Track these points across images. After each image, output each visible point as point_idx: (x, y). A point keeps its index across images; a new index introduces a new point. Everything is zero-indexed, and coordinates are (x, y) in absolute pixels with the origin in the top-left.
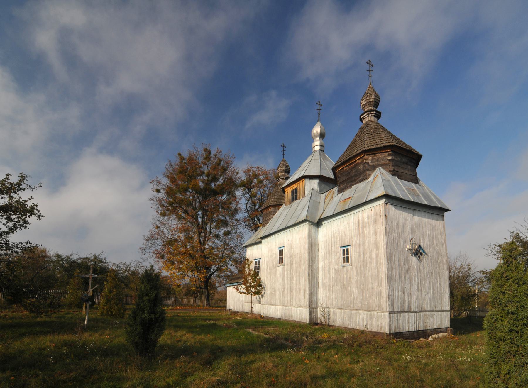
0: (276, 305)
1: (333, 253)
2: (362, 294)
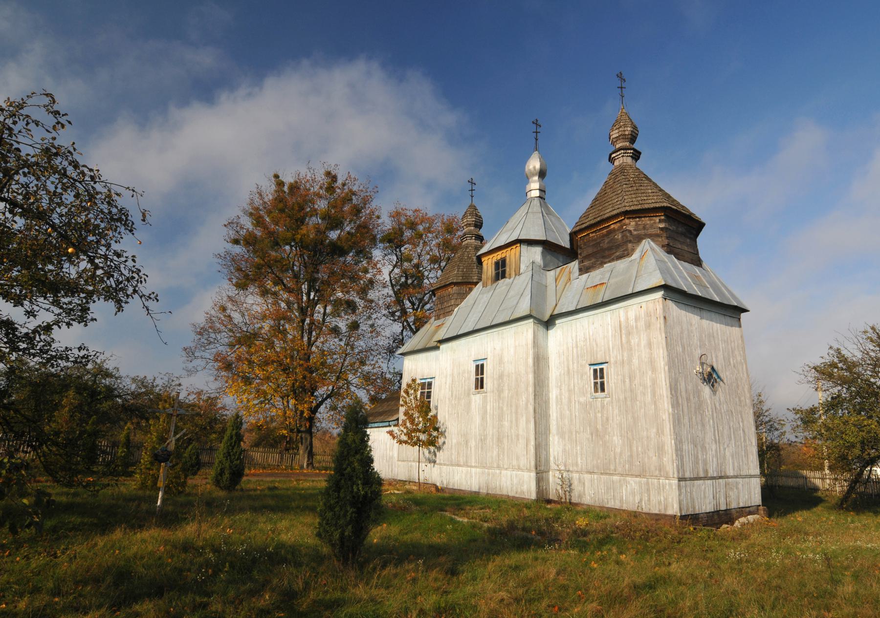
0: (468, 466)
1: (575, 374)
2: (631, 447)
